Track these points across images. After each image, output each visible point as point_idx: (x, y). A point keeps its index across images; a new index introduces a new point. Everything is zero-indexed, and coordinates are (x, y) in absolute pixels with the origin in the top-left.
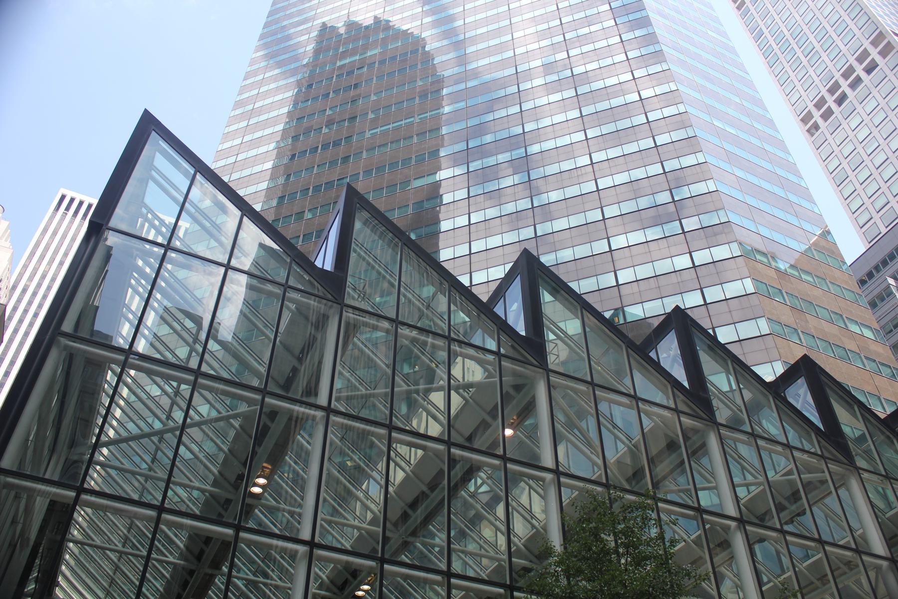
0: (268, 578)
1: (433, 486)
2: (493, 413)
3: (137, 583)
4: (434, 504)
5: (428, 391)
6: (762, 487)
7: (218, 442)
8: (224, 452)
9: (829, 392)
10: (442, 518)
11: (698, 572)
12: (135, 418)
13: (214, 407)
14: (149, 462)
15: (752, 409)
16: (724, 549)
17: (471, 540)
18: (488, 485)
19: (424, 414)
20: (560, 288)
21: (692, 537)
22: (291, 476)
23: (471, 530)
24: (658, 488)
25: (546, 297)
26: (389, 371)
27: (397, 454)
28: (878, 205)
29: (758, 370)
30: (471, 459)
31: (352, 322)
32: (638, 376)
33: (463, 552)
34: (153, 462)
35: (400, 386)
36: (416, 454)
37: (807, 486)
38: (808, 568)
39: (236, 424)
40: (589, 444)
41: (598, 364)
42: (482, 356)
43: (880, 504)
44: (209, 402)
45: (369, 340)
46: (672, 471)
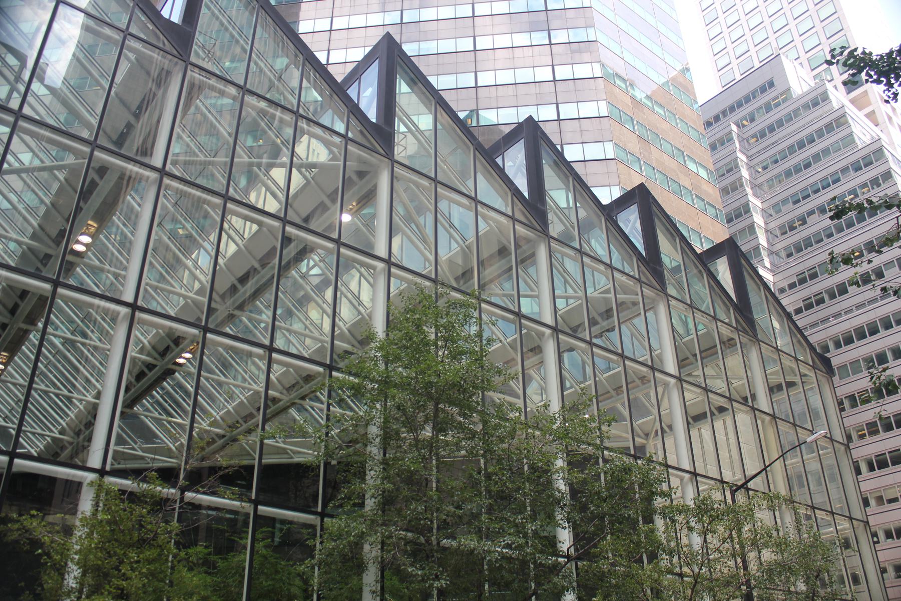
0: (87, 338)
1: (264, 262)
2: (332, 197)
5: (271, 166)
6: (580, 302)
7: (40, 194)
8: (46, 204)
9: (657, 222)
10: (269, 296)
13: (38, 157)
15: (583, 228)
16: (536, 354)
17: (297, 320)
19: (264, 189)
20: (418, 80)
21: (508, 340)
22: (118, 238)
23: (298, 310)
24: (483, 290)
25: (402, 87)
26: (231, 140)
27: (232, 226)
28: (739, 52)
29: (597, 191)
30: (305, 240)
31: (197, 82)
32: (480, 177)
35: (240, 157)
36: (251, 228)
39: (61, 176)
40: (424, 241)
41: (444, 162)
42: (328, 137)
43: (680, 329)
44: (32, 150)
45: (214, 106)
46: (499, 276)
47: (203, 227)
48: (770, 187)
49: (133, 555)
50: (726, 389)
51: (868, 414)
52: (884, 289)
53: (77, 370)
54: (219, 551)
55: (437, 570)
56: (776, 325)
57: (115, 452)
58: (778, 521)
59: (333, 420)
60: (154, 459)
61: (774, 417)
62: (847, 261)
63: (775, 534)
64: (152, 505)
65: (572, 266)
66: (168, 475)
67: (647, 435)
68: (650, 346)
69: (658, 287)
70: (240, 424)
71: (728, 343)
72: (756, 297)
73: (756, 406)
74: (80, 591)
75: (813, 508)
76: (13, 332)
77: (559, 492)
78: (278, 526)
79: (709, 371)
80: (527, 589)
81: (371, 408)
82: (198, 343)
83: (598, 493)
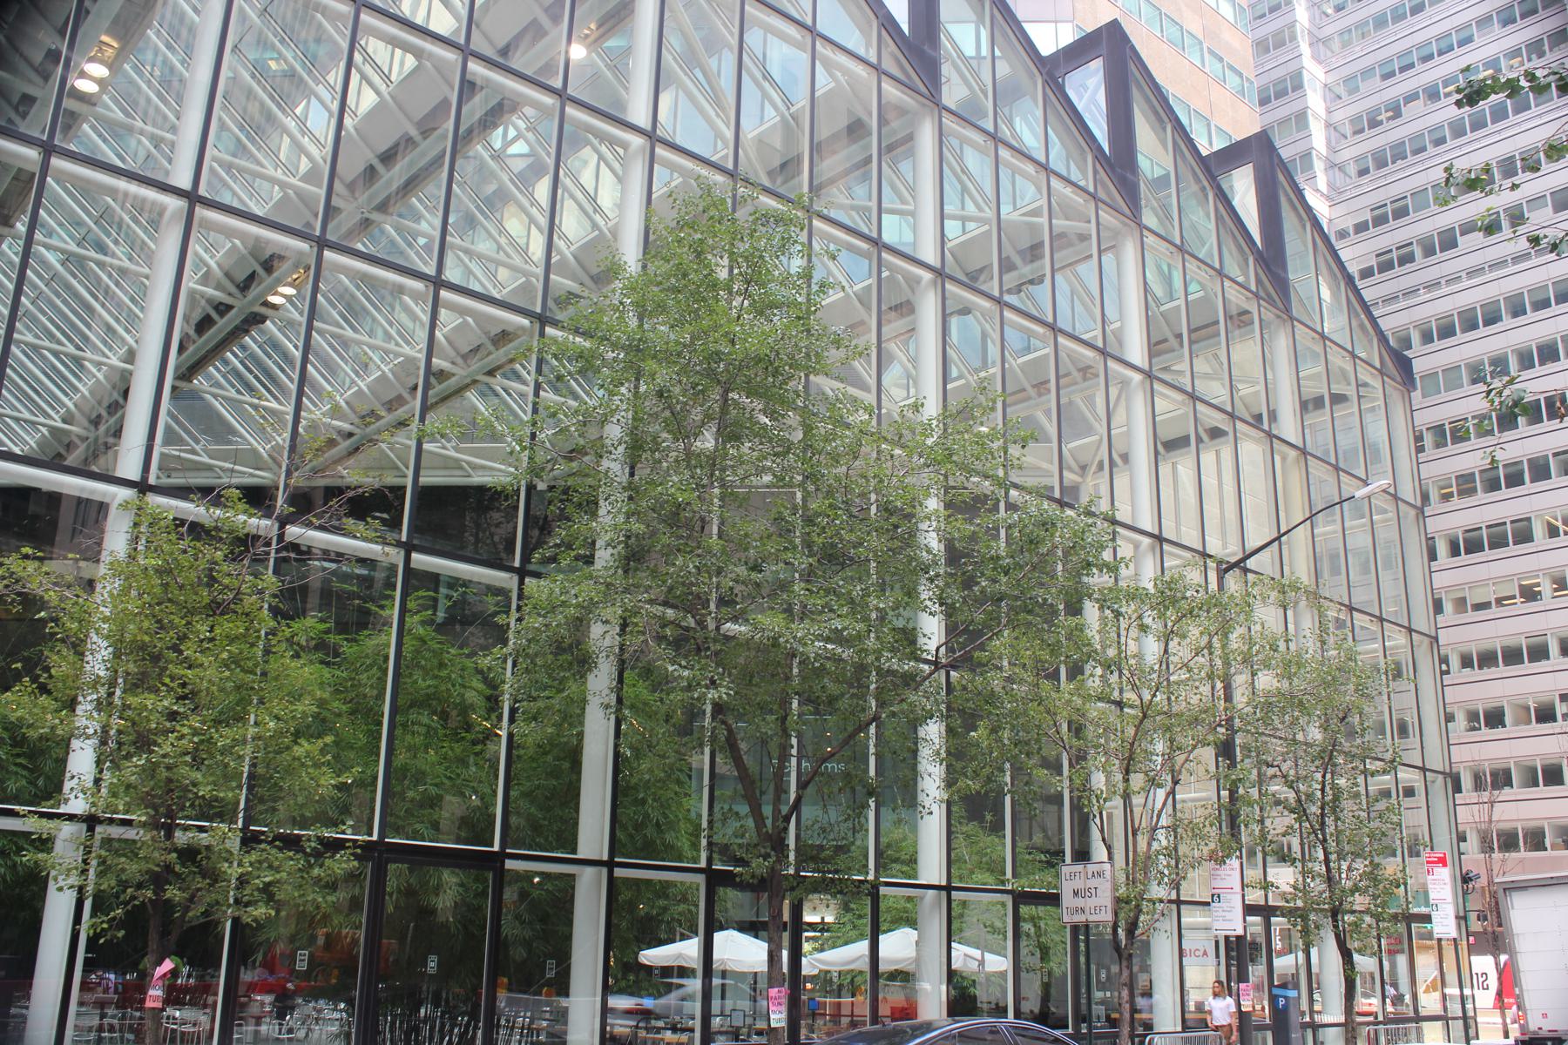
4: (428, 158)
6: (986, 227)
10: (435, 189)
15: (1002, 95)
16: (902, 315)
18: (527, 141)
21: (856, 288)
22: (157, 73)
27: (369, 59)
29: (1032, 30)
30: (499, 88)
33: (467, 251)
36: (402, 64)
37: (1058, 238)
38: (1022, 367)
40: (717, 101)
43: (1158, 289)
46: (847, 172)
47: (315, 57)
48: (1345, 45)
49: (202, 628)
50: (1227, 398)
51: (1469, 458)
52: (1535, 241)
54: (342, 628)
55: (713, 671)
56: (1326, 294)
57: (162, 455)
58: (1291, 627)
59: (542, 413)
60: (232, 470)
61: (1304, 452)
62: (1472, 185)
63: (1282, 646)
64: (231, 544)
65: (976, 163)
66: (257, 497)
67: (1084, 468)
68: (1103, 314)
69: (1127, 212)
70: (368, 422)
71: (1240, 319)
72: (1296, 241)
73: (1274, 432)
74: (112, 683)
75: (1351, 609)
77: (929, 551)
78: (443, 590)
79: (1201, 366)
80: (864, 710)
81: (611, 394)
82: (307, 268)
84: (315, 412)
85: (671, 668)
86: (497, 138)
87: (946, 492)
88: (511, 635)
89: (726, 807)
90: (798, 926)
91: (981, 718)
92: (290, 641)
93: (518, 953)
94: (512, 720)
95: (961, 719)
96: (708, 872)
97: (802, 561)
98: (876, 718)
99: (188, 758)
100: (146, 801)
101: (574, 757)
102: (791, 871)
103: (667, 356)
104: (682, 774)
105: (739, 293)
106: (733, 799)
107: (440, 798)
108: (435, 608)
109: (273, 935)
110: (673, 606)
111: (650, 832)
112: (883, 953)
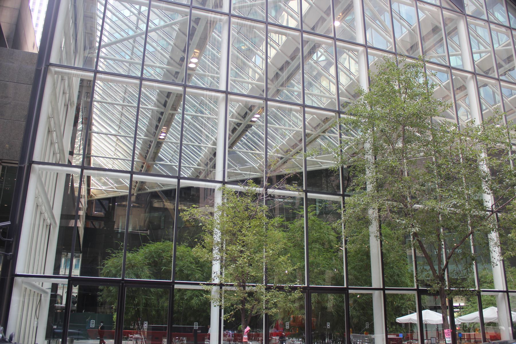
1: (293, 58)
3: (135, 122)
6: (489, 54)
10: (298, 76)
11: (447, 103)
12: (118, 30)
13: (162, 19)
14: (130, 55)
16: (462, 91)
19: (286, 15)
21: (443, 84)
22: (210, 57)
27: (272, 40)
30: (313, 41)
33: (310, 94)
34: (132, 55)
38: (510, 102)
39: (176, 28)
40: (386, 30)
46: (434, 45)
47: (255, 42)
53: (201, 131)
54: (288, 219)
57: (228, 172)
65: (482, 32)
66: (257, 181)
68: (501, 93)
76: (166, 116)
77: (484, 172)
78: (317, 204)
81: (365, 133)
83: (510, 171)
84: (270, 153)
85: (398, 221)
86: (315, 57)
87: (488, 151)
88: (342, 216)
89: (422, 267)
90: (452, 308)
91: (512, 229)
92: (273, 225)
93: (355, 320)
94: (346, 244)
95: (504, 230)
96: (417, 290)
97: (438, 181)
98: (472, 233)
99: (247, 264)
100: (237, 278)
101: (367, 254)
102: (447, 288)
103: (382, 118)
104: (404, 257)
105: (403, 93)
106: (424, 265)
107: (325, 271)
108: (316, 210)
109: (277, 318)
110: (395, 201)
111: (396, 278)
112: (485, 316)
